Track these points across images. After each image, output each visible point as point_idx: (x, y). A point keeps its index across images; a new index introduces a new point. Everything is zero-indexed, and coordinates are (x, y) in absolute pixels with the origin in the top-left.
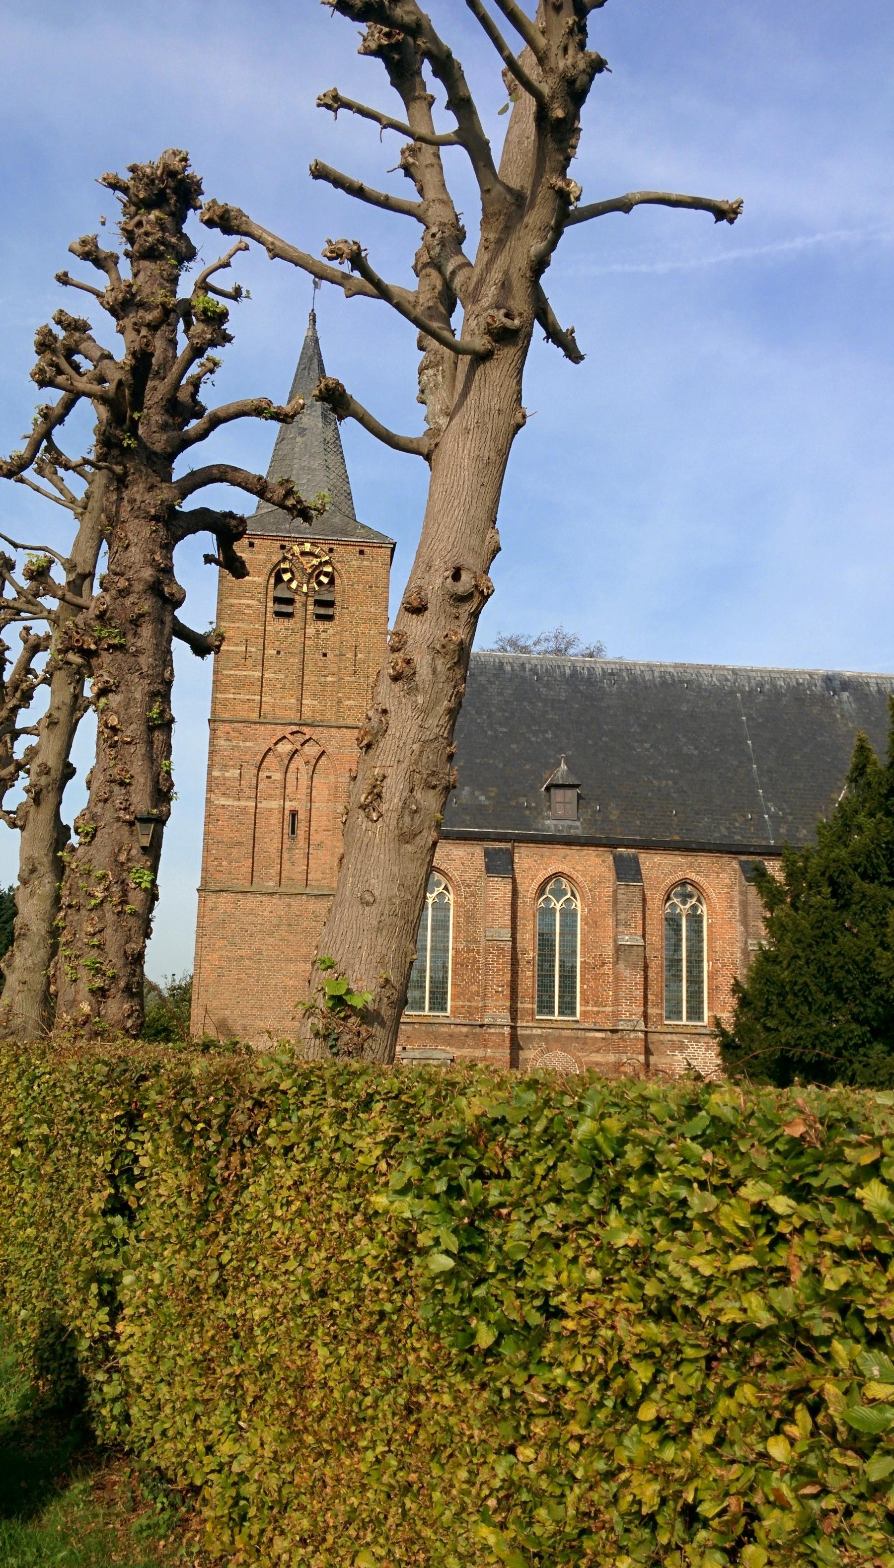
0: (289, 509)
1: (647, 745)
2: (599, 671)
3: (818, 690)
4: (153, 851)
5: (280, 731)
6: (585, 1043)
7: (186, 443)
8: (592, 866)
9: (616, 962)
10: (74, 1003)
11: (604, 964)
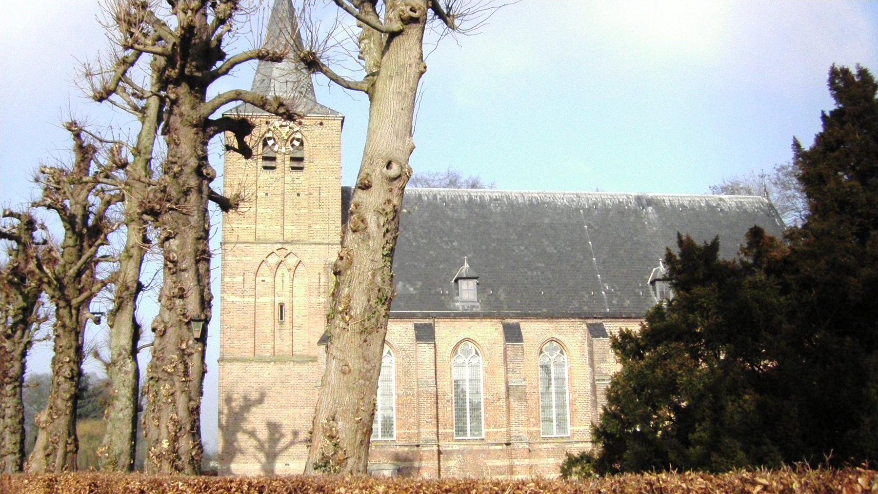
0: (281, 115)
1: (523, 248)
2: (487, 198)
3: (632, 205)
4: (202, 339)
6: (489, 454)
7: (216, 76)
8: (490, 332)
9: (508, 397)
10: (158, 441)
11: (499, 399)
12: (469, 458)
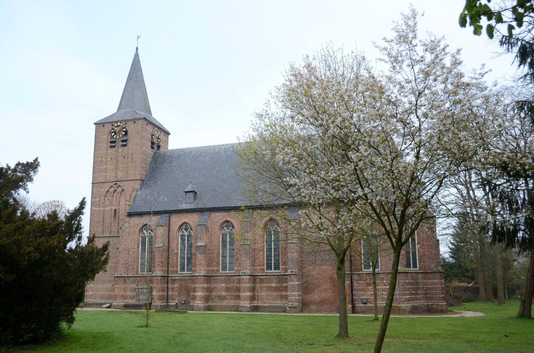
5: (111, 184)
12: (183, 283)
